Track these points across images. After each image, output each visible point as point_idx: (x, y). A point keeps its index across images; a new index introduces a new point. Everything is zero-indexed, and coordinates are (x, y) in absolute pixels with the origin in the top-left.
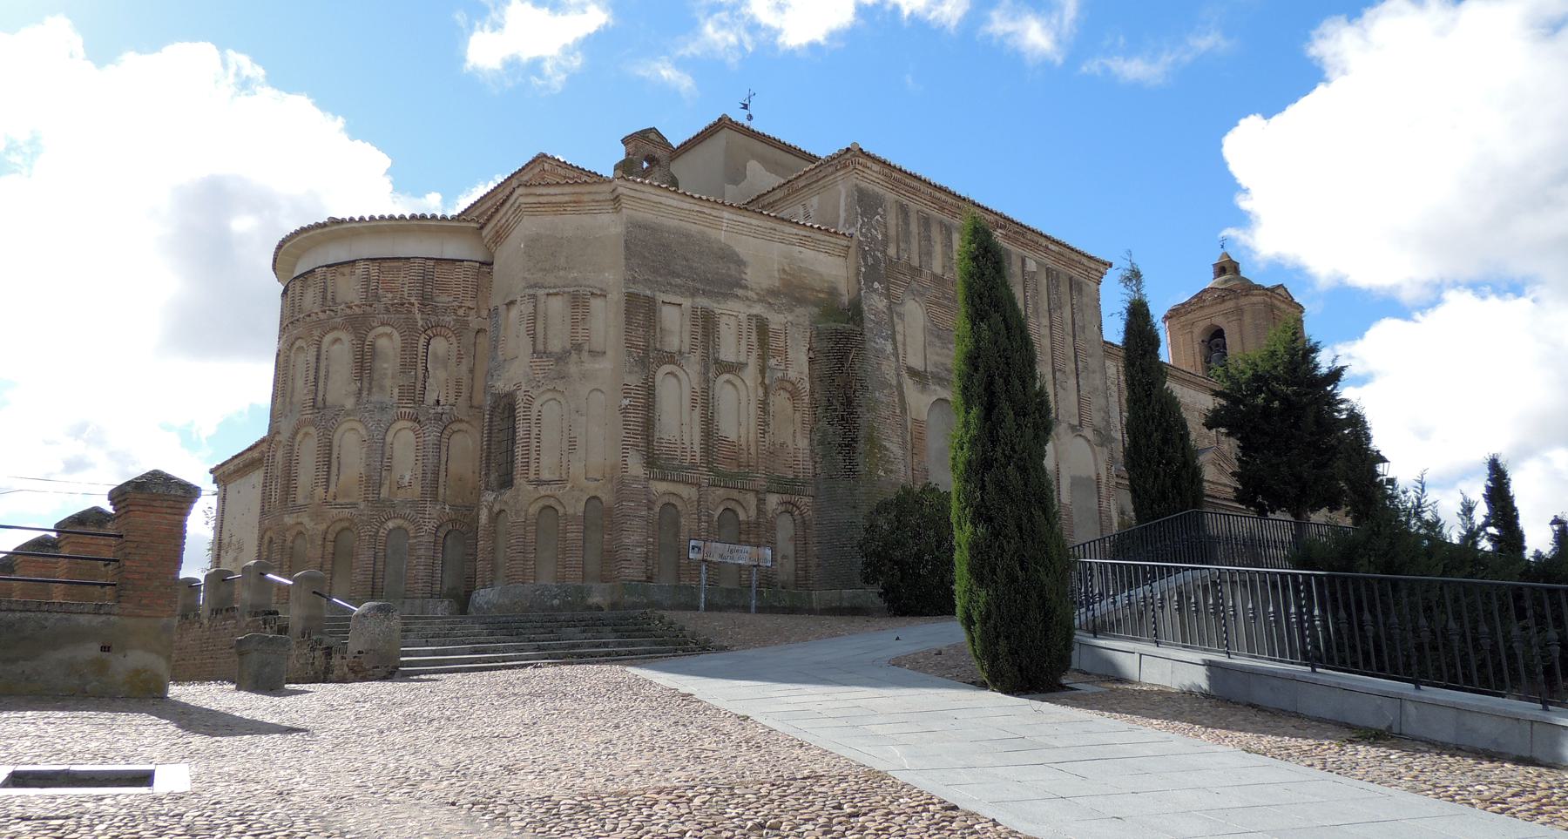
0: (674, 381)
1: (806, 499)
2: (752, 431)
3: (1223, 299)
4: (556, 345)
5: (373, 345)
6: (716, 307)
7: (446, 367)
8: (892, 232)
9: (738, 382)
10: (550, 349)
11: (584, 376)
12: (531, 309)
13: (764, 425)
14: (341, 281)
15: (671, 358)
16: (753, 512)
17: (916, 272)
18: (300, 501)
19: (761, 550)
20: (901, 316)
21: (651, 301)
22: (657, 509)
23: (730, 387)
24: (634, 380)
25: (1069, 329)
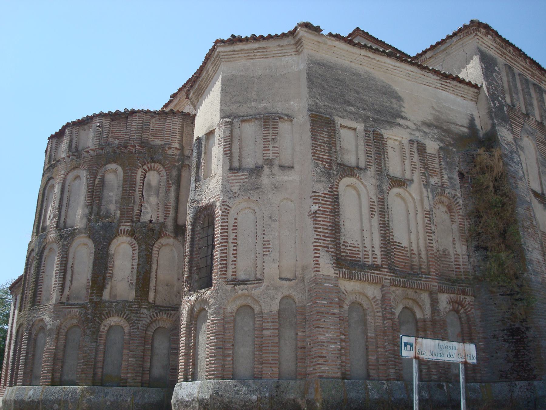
0: (354, 192)
2: (421, 236)
4: (250, 162)
5: (103, 179)
7: (157, 195)
11: (276, 187)
13: (429, 232)
14: (82, 133)
15: (349, 171)
16: (428, 312)
22: (346, 307)
23: (399, 200)
24: (322, 188)
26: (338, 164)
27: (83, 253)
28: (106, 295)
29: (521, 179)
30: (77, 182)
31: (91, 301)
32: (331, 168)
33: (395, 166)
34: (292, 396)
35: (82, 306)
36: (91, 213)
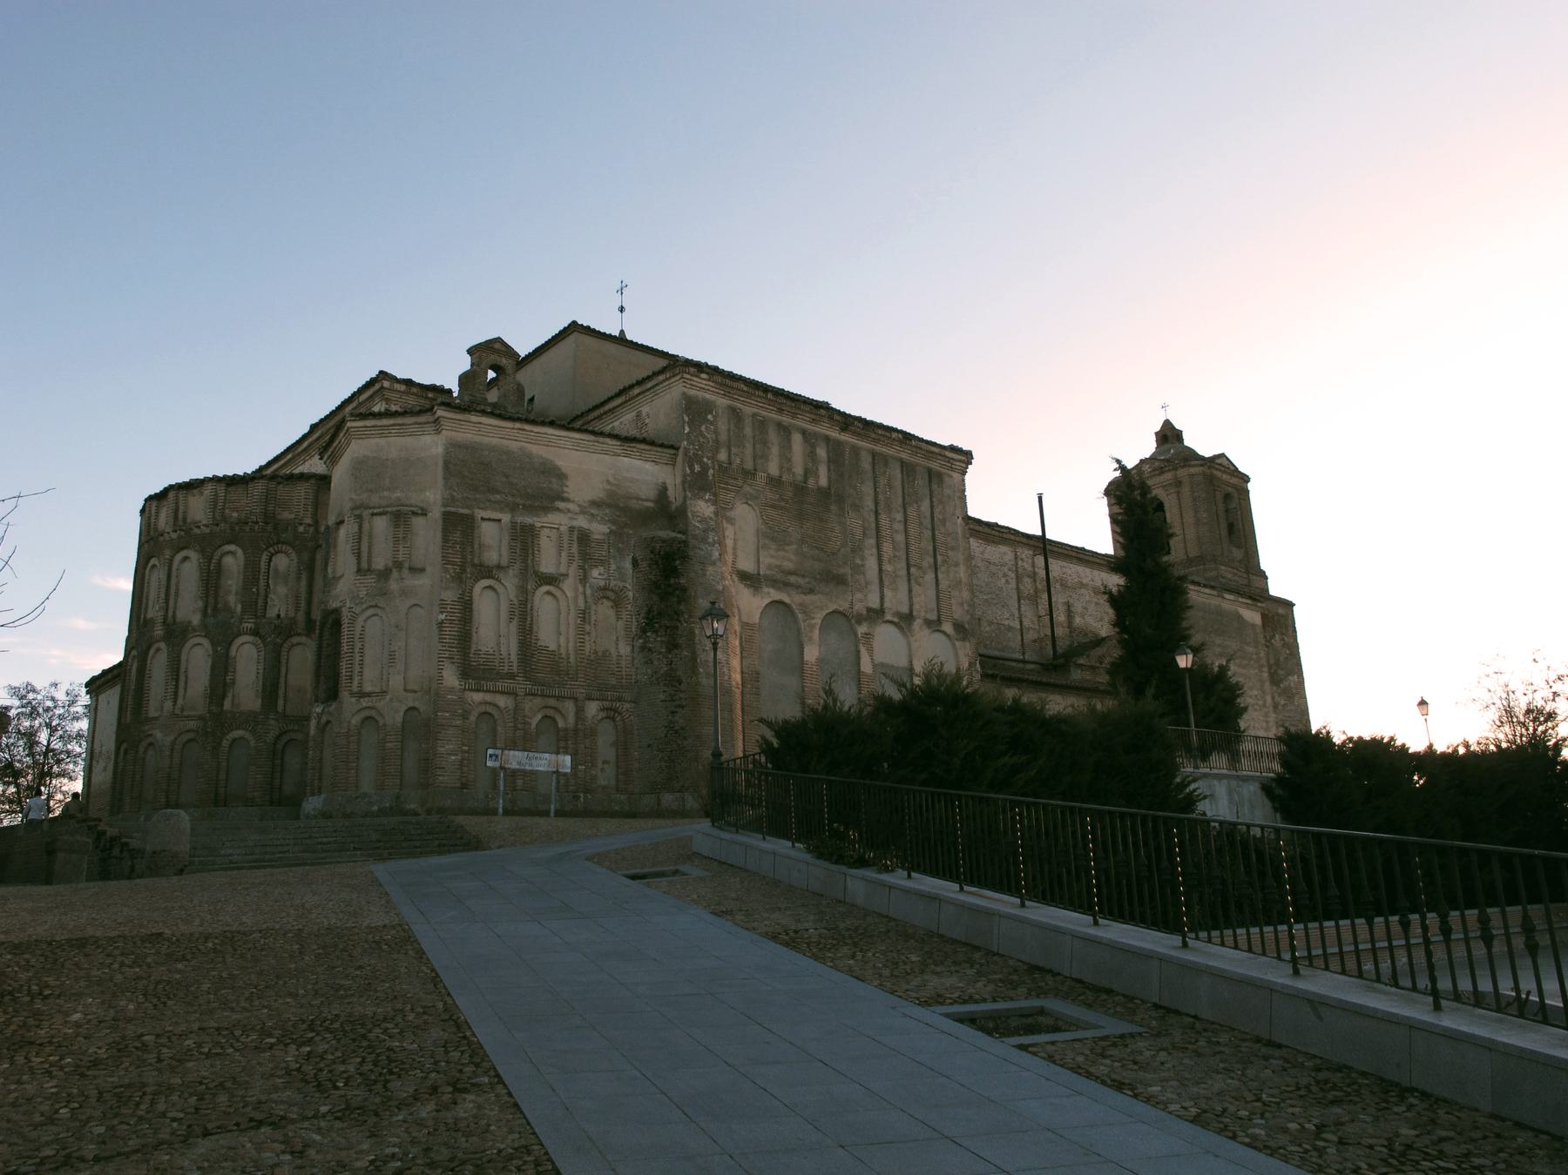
1: (627, 706)
3: (1161, 471)
4: (380, 563)
5: (219, 563)
6: (537, 521)
8: (723, 437)
9: (558, 593)
10: (374, 566)
11: (404, 593)
12: (356, 529)
13: (582, 633)
15: (486, 572)
16: (571, 719)
17: (749, 475)
18: (153, 713)
19: (561, 757)
20: (731, 521)
21: (471, 518)
22: (473, 718)
23: (548, 598)
24: (450, 595)
25: (927, 522)
26: (474, 565)
27: (198, 657)
28: (227, 705)
29: (714, 564)
30: (186, 564)
31: (210, 712)
32: (463, 570)
33: (548, 561)
34: (413, 806)
35: (201, 718)
36: (206, 607)
